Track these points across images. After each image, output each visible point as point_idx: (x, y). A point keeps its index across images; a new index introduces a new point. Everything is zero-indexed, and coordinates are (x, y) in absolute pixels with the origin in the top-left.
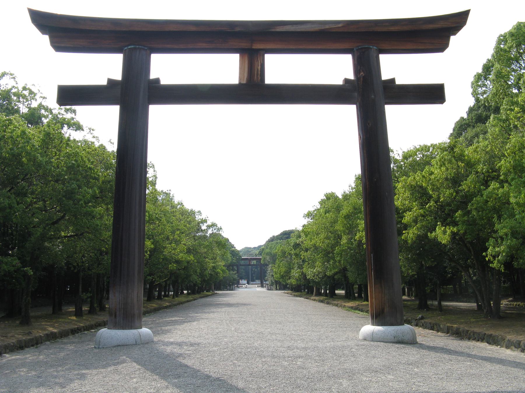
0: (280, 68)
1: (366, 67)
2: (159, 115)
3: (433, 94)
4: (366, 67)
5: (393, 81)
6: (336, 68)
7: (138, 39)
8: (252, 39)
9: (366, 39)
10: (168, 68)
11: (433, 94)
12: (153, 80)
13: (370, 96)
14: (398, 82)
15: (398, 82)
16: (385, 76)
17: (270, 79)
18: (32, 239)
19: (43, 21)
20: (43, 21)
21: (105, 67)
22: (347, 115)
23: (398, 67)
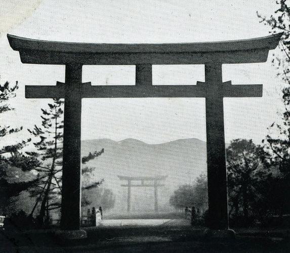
0: (162, 74)
1: (213, 73)
2: (87, 104)
3: (255, 91)
4: (213, 73)
5: (230, 82)
6: (194, 74)
7: (74, 57)
8: (142, 57)
9: (211, 55)
10: (92, 74)
11: (255, 91)
12: (66, 82)
13: (214, 92)
14: (233, 84)
15: (233, 84)
16: (84, 80)
17: (157, 80)
18: (74, 233)
19: (15, 42)
20: (15, 42)
21: (54, 74)
22: (201, 102)
23: (232, 73)
